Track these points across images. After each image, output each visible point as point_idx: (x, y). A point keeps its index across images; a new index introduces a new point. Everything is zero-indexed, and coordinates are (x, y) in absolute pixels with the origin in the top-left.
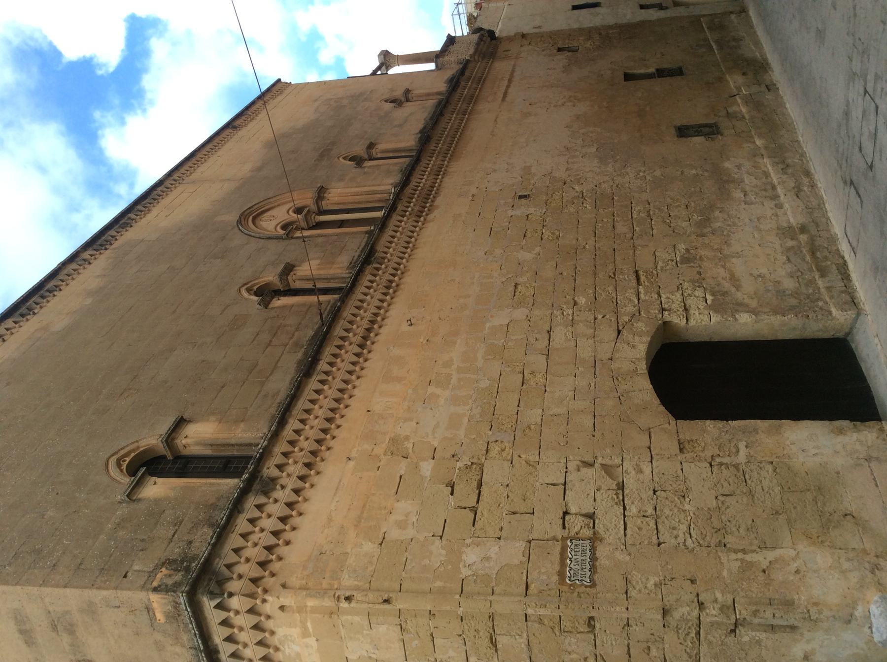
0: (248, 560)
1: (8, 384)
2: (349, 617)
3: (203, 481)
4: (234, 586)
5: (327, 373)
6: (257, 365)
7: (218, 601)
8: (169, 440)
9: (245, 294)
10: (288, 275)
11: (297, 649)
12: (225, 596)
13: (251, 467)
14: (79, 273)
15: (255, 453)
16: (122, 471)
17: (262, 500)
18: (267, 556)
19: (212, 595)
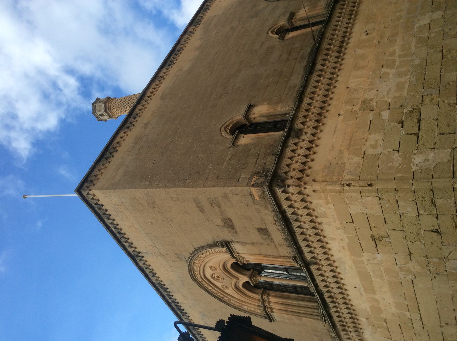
1: (170, 99)
2: (350, 194)
4: (289, 182)
5: (321, 70)
6: (283, 72)
9: (271, 34)
10: (292, 19)
11: (324, 210)
12: (286, 186)
13: (288, 125)
15: (289, 117)
16: (227, 133)
17: (296, 140)
18: (303, 167)
19: (280, 187)
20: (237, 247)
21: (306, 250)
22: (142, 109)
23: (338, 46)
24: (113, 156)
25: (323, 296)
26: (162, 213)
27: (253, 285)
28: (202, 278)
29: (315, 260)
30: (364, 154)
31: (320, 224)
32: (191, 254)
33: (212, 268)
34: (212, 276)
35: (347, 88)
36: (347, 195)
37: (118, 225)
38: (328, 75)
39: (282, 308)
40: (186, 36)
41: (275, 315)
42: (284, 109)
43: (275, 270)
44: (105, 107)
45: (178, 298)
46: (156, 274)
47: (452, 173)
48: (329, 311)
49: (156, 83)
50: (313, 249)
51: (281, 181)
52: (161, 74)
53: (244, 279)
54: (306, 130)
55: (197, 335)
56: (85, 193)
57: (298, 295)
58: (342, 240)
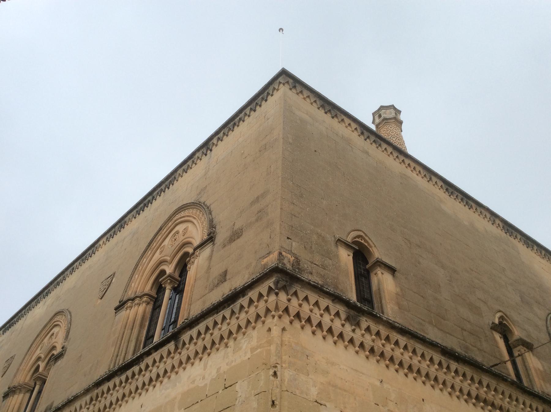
0: (300, 305)
1: (401, 183)
2: (263, 377)
3: (353, 282)
4: (283, 296)
5: (448, 368)
6: (445, 320)
7: (273, 287)
8: (379, 263)
9: (498, 315)
10: (523, 345)
11: (244, 347)
12: (277, 291)
13: (365, 308)
14: (484, 218)
15: (376, 311)
16: (355, 238)
17: (343, 316)
18: (304, 319)
19: (276, 283)
20: (207, 251)
21: (194, 332)
22: (387, 152)
23: (487, 398)
24: (326, 113)
25: (136, 364)
26: (254, 161)
27: (160, 280)
28: (176, 221)
29: (180, 345)
30: (321, 405)
31: (226, 346)
32: (204, 203)
33: (186, 229)
34: (178, 232)
35: (423, 400)
36: (262, 373)
37: (243, 121)
38: (441, 377)
39: (129, 320)
40: (488, 215)
41: (123, 313)
42: (390, 312)
43: (177, 308)
44: (390, 119)
45: (156, 204)
46: (186, 172)
47: (213, 258)
48: (117, 375)
49: (422, 171)
50: (195, 340)
51: (285, 286)
52: (434, 179)
53: (169, 269)
54: (358, 331)
55: (113, 231)
56: (281, 79)
57: (143, 341)
58: (204, 378)
